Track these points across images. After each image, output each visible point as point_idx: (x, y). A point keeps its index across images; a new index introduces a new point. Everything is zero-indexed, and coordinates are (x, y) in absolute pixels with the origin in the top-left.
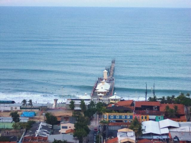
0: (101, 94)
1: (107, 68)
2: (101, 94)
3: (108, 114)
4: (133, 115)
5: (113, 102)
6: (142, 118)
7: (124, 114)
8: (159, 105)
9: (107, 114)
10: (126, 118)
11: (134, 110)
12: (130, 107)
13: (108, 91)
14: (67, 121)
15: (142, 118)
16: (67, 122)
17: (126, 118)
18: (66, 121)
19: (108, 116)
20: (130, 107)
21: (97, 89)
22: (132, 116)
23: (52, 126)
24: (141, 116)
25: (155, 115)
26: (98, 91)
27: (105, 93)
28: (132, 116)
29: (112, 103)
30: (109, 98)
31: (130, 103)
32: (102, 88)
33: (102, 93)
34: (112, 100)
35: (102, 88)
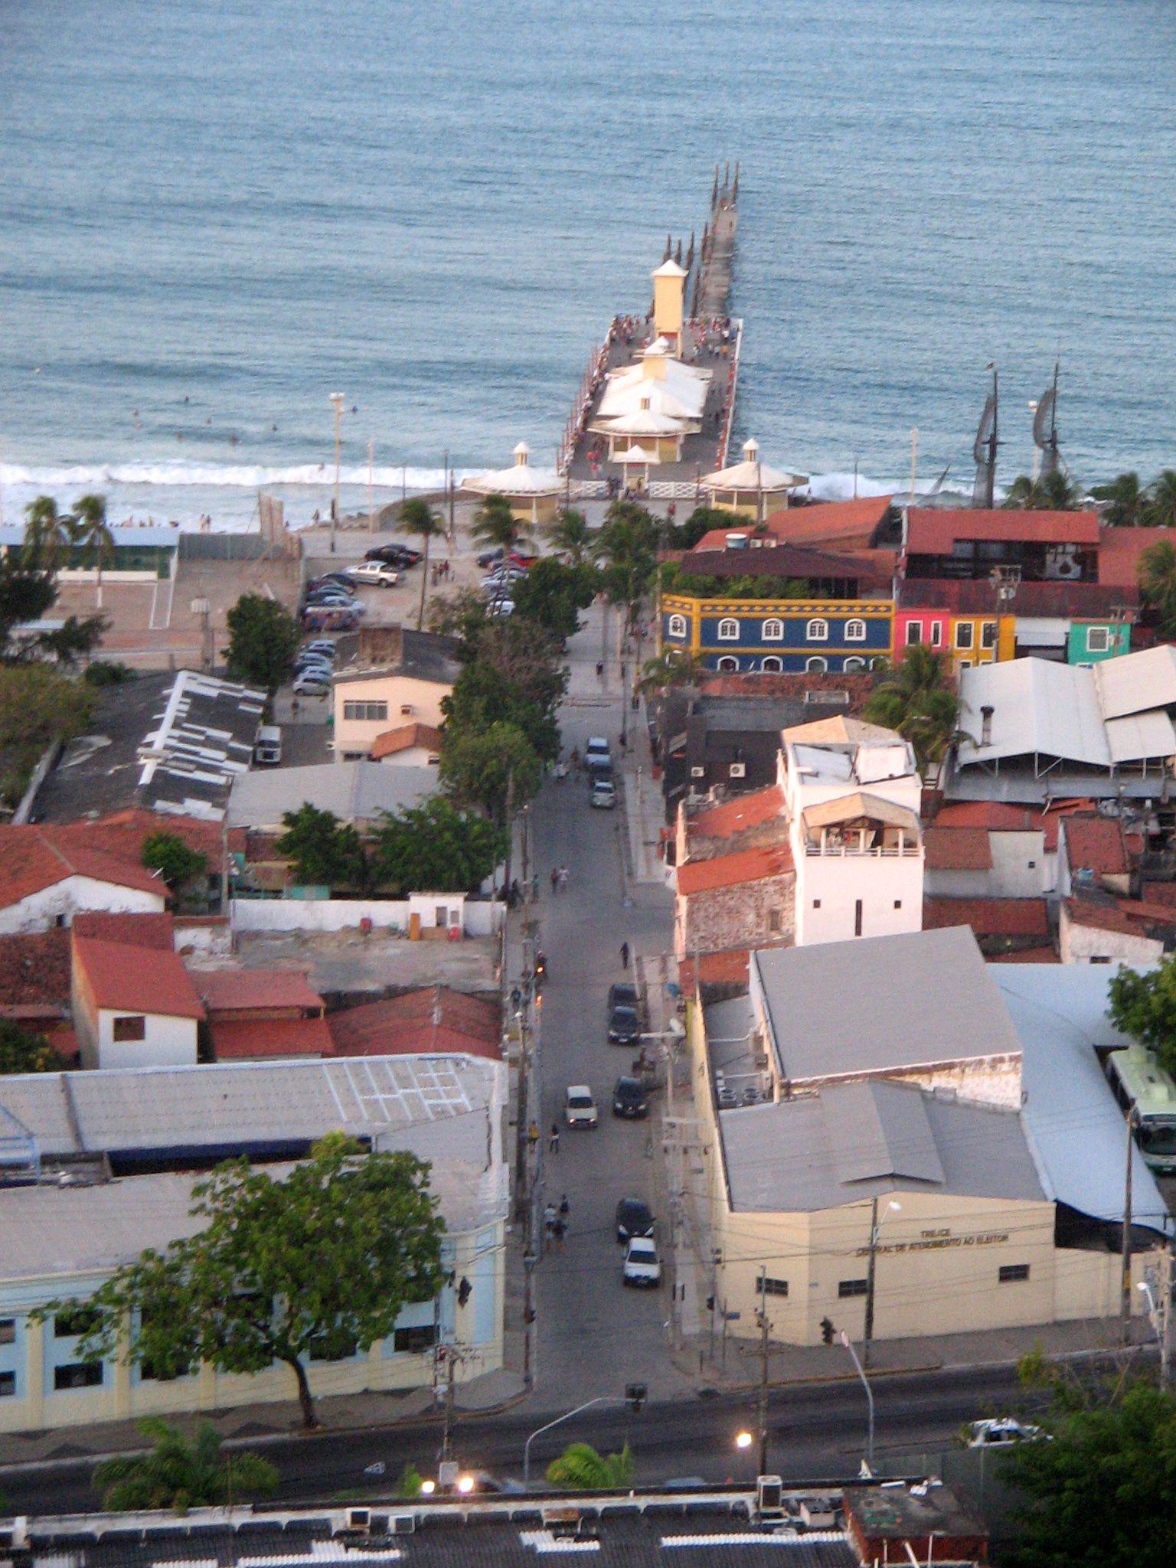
0: (635, 454)
1: (674, 248)
2: (635, 454)
3: (696, 608)
4: (891, 614)
5: (732, 508)
6: (964, 639)
7: (789, 608)
8: (1096, 540)
9: (695, 603)
10: (836, 638)
11: (903, 575)
12: (871, 554)
13: (696, 429)
14: (382, 660)
15: (964, 639)
16: (384, 668)
17: (836, 638)
18: (374, 661)
19: (696, 621)
20: (871, 554)
21: (605, 409)
22: (887, 621)
23: (263, 696)
24: (956, 624)
25: (1062, 614)
26: (612, 424)
27: (670, 437)
28: (887, 621)
29: (729, 522)
30: (702, 486)
31: (873, 519)
32: (646, 403)
33: (645, 441)
34: (726, 496)
35: (646, 403)
